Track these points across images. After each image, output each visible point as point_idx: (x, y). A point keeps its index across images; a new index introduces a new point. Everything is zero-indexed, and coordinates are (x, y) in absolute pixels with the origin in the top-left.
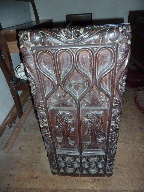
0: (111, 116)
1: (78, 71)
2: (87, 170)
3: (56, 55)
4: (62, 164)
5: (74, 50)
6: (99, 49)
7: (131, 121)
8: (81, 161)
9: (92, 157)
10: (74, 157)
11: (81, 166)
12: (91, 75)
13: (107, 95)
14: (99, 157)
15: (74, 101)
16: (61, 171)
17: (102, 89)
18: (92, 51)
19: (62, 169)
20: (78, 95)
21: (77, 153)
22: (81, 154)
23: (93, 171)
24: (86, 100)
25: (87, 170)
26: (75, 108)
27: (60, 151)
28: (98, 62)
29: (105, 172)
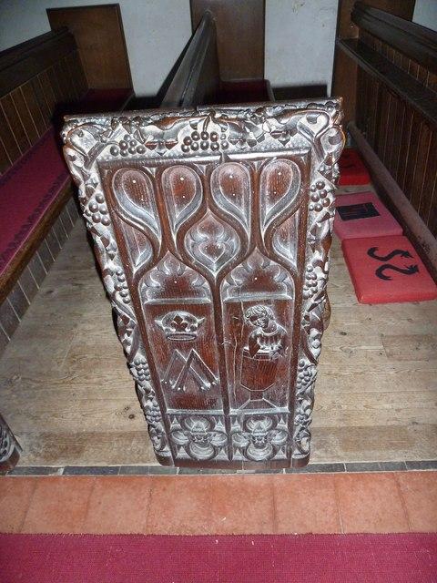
0: (290, 406)
1: (214, 208)
2: (244, 451)
4: (182, 439)
7: (318, 165)
10: (274, 419)
11: (229, 441)
12: (248, 218)
15: (206, 284)
16: (234, 457)
17: (279, 256)
18: (248, 162)
19: (182, 449)
20: (215, 267)
24: (235, 279)
25: (244, 451)
26: (207, 300)
28: (142, 218)
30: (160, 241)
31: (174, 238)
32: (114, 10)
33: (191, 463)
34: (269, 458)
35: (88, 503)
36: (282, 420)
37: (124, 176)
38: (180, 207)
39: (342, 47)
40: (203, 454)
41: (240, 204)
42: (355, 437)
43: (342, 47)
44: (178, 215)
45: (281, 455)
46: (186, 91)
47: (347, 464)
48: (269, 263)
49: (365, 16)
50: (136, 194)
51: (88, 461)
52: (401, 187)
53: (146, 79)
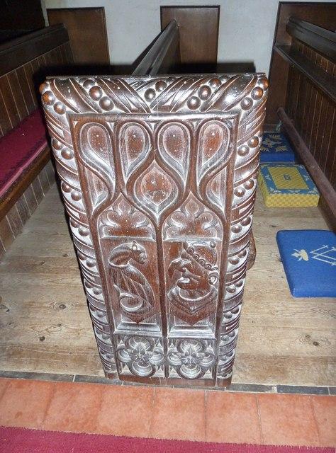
1: (160, 162)
3: (157, 134)
5: (153, 125)
6: (202, 121)
8: (166, 350)
9: (188, 340)
13: (216, 211)
14: (201, 343)
17: (210, 203)
19: (126, 366)
21: (157, 331)
22: (165, 333)
23: (192, 374)
27: (122, 327)
29: (214, 375)
30: (185, 185)
31: (198, 184)
32: (280, 3)
33: (135, 378)
34: (199, 376)
35: (314, 418)
36: (210, 346)
37: (130, 128)
38: (133, 156)
39: (277, 50)
40: (142, 372)
41: (207, 158)
42: (277, 364)
43: (277, 50)
44: (129, 165)
45: (209, 375)
46: (157, 65)
47: (330, 388)
48: (203, 209)
49: (299, 28)
50: (98, 145)
51: (287, 383)
52: (312, 154)
53: (123, 48)
